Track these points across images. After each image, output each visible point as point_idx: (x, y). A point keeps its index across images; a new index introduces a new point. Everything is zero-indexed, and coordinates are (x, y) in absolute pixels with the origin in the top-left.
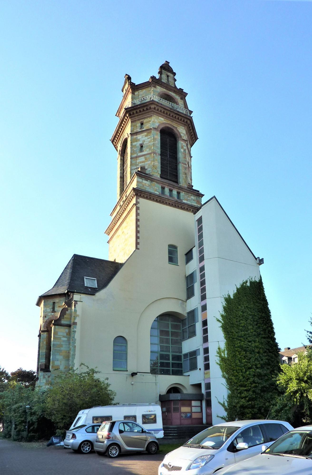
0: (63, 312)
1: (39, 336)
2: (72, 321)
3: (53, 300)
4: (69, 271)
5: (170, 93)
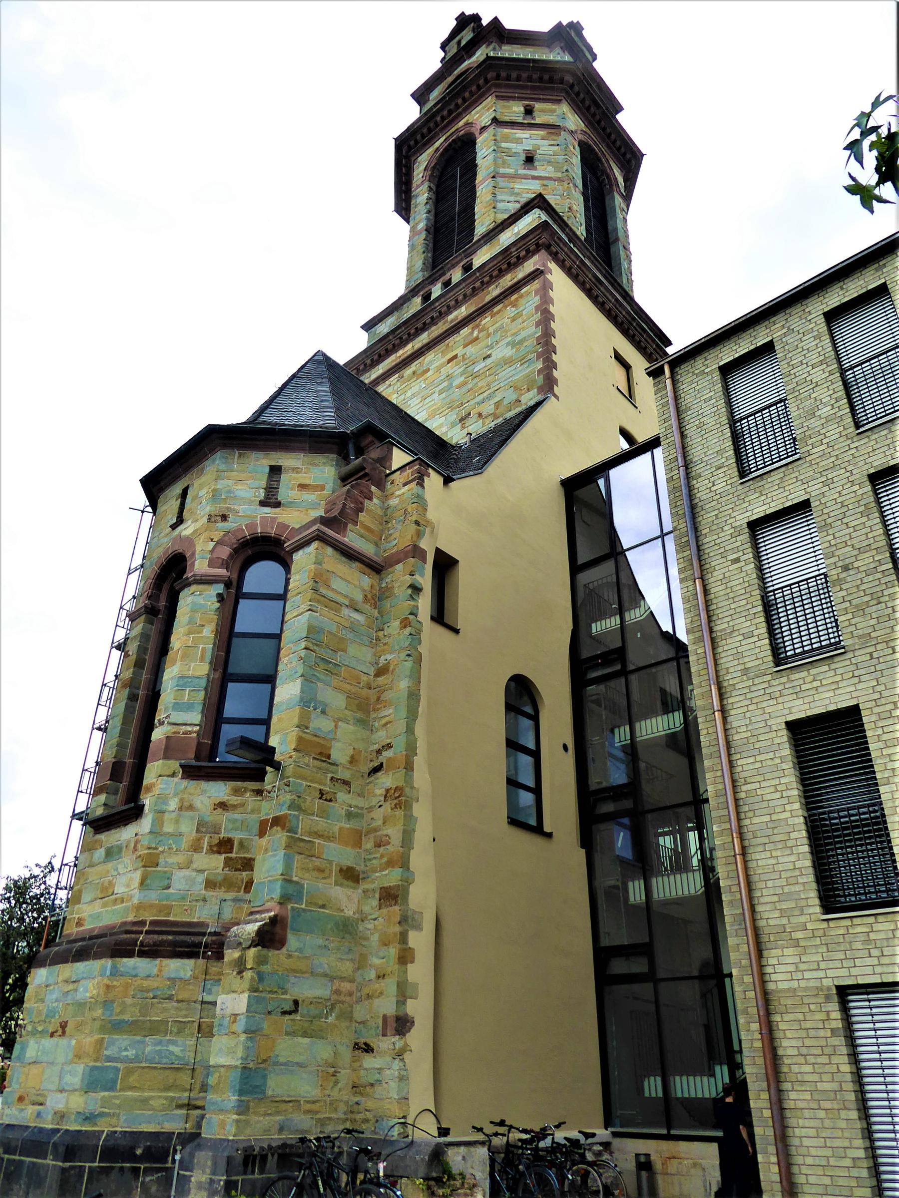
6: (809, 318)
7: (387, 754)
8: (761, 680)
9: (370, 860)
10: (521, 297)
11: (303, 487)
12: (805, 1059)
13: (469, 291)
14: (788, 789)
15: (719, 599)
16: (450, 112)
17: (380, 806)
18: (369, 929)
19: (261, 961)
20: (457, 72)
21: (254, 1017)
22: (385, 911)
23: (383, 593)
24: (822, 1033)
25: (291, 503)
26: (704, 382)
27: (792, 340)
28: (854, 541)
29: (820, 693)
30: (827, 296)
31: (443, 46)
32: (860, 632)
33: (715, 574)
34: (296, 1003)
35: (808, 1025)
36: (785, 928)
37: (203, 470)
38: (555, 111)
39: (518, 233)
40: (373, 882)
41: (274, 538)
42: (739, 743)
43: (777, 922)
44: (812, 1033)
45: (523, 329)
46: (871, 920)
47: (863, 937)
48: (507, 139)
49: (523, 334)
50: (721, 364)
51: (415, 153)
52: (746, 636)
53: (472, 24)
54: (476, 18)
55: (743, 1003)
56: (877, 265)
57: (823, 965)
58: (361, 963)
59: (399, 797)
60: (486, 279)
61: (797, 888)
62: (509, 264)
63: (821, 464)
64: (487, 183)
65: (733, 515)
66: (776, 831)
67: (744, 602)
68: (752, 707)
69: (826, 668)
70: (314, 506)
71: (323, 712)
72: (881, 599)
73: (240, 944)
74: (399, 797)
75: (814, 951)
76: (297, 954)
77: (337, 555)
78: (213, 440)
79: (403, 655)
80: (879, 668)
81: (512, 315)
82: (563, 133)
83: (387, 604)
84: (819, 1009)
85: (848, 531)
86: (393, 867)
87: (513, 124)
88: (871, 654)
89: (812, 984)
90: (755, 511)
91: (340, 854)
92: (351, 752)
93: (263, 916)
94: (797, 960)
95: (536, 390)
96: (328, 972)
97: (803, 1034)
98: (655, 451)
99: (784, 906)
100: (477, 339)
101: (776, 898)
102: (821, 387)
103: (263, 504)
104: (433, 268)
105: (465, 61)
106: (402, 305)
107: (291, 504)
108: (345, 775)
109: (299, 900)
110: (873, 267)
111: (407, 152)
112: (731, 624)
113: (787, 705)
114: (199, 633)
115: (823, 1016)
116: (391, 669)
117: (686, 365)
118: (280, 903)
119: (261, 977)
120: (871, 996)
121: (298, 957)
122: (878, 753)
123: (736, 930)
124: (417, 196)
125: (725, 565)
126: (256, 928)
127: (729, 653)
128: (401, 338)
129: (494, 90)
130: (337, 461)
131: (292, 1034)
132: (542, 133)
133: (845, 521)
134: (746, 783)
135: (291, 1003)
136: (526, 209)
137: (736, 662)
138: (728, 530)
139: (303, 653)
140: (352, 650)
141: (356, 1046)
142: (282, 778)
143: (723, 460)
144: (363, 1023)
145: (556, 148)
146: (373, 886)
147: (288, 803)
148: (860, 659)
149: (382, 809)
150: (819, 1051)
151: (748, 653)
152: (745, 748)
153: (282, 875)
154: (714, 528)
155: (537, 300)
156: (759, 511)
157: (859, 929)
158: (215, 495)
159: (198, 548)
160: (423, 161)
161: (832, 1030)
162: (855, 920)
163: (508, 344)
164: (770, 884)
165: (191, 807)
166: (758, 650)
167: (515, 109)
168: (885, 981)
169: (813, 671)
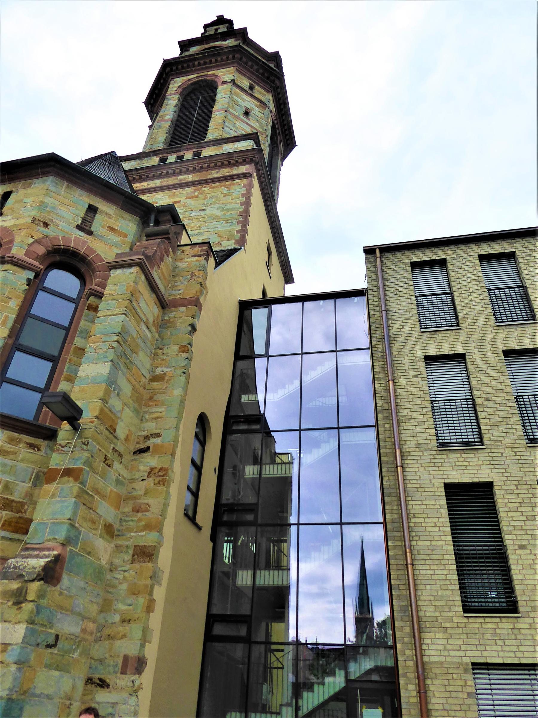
6: (470, 254)
7: (158, 441)
8: (428, 453)
9: (127, 521)
10: (234, 184)
11: (111, 229)
12: (448, 713)
13: (198, 167)
14: (444, 526)
15: (402, 397)
16: (205, 63)
17: (143, 480)
18: (117, 579)
19: (41, 595)
20: (212, 44)
21: (26, 648)
22: (137, 566)
23: (165, 324)
24: (461, 695)
25: (101, 236)
26: (399, 267)
27: (458, 263)
28: (493, 385)
29: (469, 469)
30: (481, 246)
32: (495, 439)
33: (400, 381)
34: (57, 637)
35: (451, 688)
36: (437, 619)
37: (30, 185)
38: (265, 95)
39: (237, 148)
40: (128, 539)
41: (82, 255)
42: (411, 490)
43: (432, 614)
44: (454, 695)
45: (232, 203)
46: (498, 620)
47: (491, 631)
48: (237, 95)
49: (230, 206)
50: (412, 261)
51: (173, 75)
52: (419, 424)
53: (227, 25)
54: (230, 23)
55: (403, 669)
56: (510, 241)
57: (463, 648)
58: (106, 607)
59: (163, 476)
60: (212, 165)
61: (448, 593)
62: (230, 163)
63: (474, 336)
64: (220, 112)
65: (415, 349)
66: (434, 553)
67: (420, 403)
68: (421, 469)
69: (473, 455)
70: (116, 245)
71: (118, 395)
72: (509, 423)
73: (22, 576)
74: (163, 476)
75: (458, 637)
76: (65, 592)
77: (146, 283)
78: (49, 165)
79: (179, 371)
80: (506, 462)
81: (225, 192)
82: (267, 109)
83: (168, 332)
84: (459, 678)
85: (489, 378)
86: (150, 531)
87: (242, 89)
88: (502, 453)
89: (455, 660)
90: (430, 351)
91: (107, 512)
92: (127, 432)
93: (51, 552)
94: (445, 642)
95: (233, 241)
96: (82, 612)
97: (447, 695)
98: (304, 303)
99: (437, 604)
100: (197, 197)
101: (432, 598)
102: (475, 294)
103: (79, 227)
104: (170, 145)
105: (219, 41)
106: (144, 157)
107: (100, 237)
108: (120, 448)
110: (508, 241)
111: (169, 72)
112: (410, 414)
113: (445, 472)
114: (6, 303)
115: (462, 683)
116: (167, 378)
117: (389, 254)
118: (63, 544)
119: (38, 610)
120: (490, 672)
121: (66, 596)
122: (505, 514)
123: (402, 616)
124: (169, 99)
125: (408, 377)
126: (43, 564)
127: (407, 431)
128: (141, 176)
129: (236, 65)
130: (139, 223)
131: (48, 666)
132: (256, 102)
133: (488, 372)
135: (53, 637)
136: (245, 137)
137: (412, 438)
138: (411, 357)
139: (115, 344)
140: (141, 354)
141: (89, 681)
142: (80, 437)
143: (411, 315)
144: (101, 661)
145: (262, 115)
146: (127, 543)
147: (84, 459)
148: (494, 455)
149: (144, 483)
150: (458, 708)
151: (420, 435)
152: (416, 494)
153: (69, 519)
154: (401, 353)
155: (244, 190)
156: (432, 352)
157: (489, 626)
158: (42, 206)
159: (17, 239)
160: (176, 84)
161: (468, 693)
162: (486, 619)
163: (219, 208)
164: (428, 587)
166: (427, 434)
167: (244, 82)
168: (506, 662)
169: (464, 455)
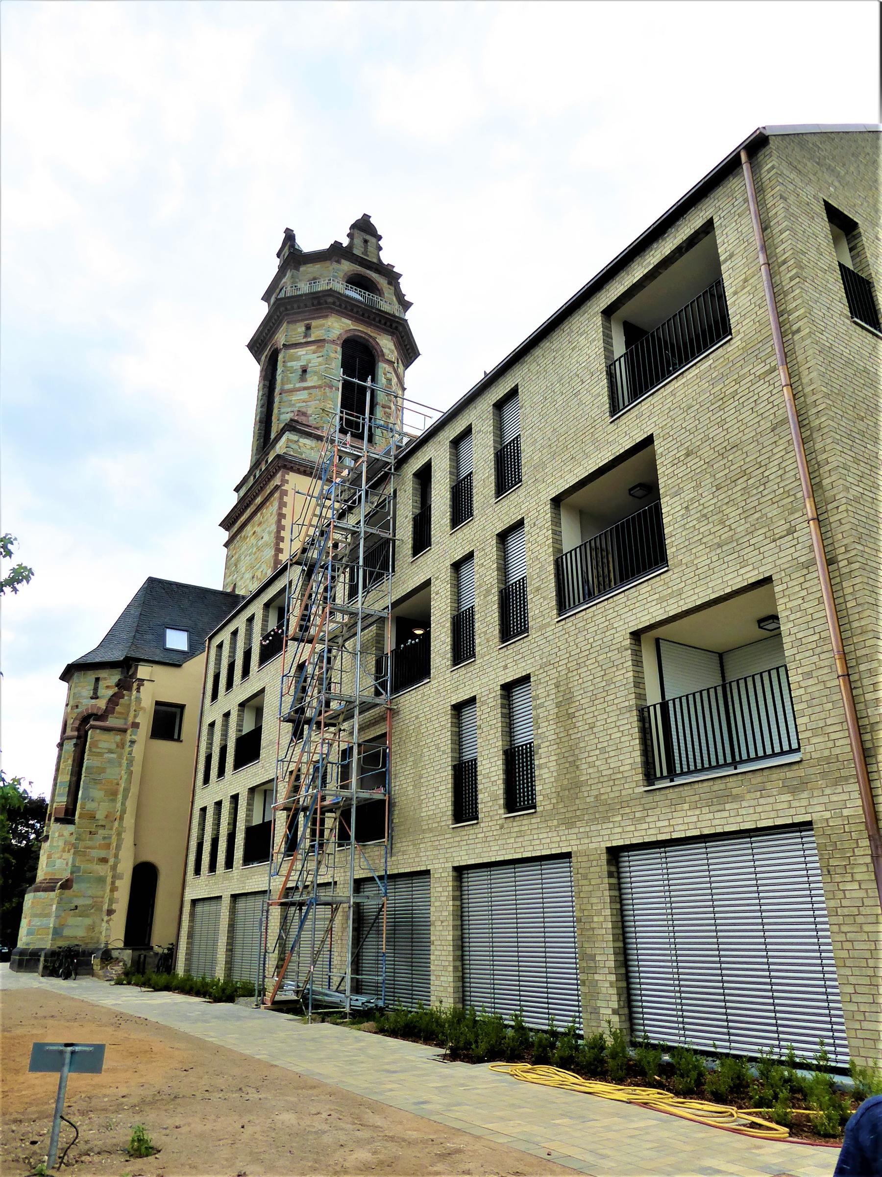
0: (114, 701)
1: (60, 745)
2: (130, 720)
3: (97, 672)
4: (136, 612)
5: (368, 272)
31: (278, 255)
38: (323, 325)
91: (97, 853)
103: (92, 698)
109: (79, 872)
131: (75, 916)
132: (313, 347)
134: (630, 706)
165: (62, 835)
